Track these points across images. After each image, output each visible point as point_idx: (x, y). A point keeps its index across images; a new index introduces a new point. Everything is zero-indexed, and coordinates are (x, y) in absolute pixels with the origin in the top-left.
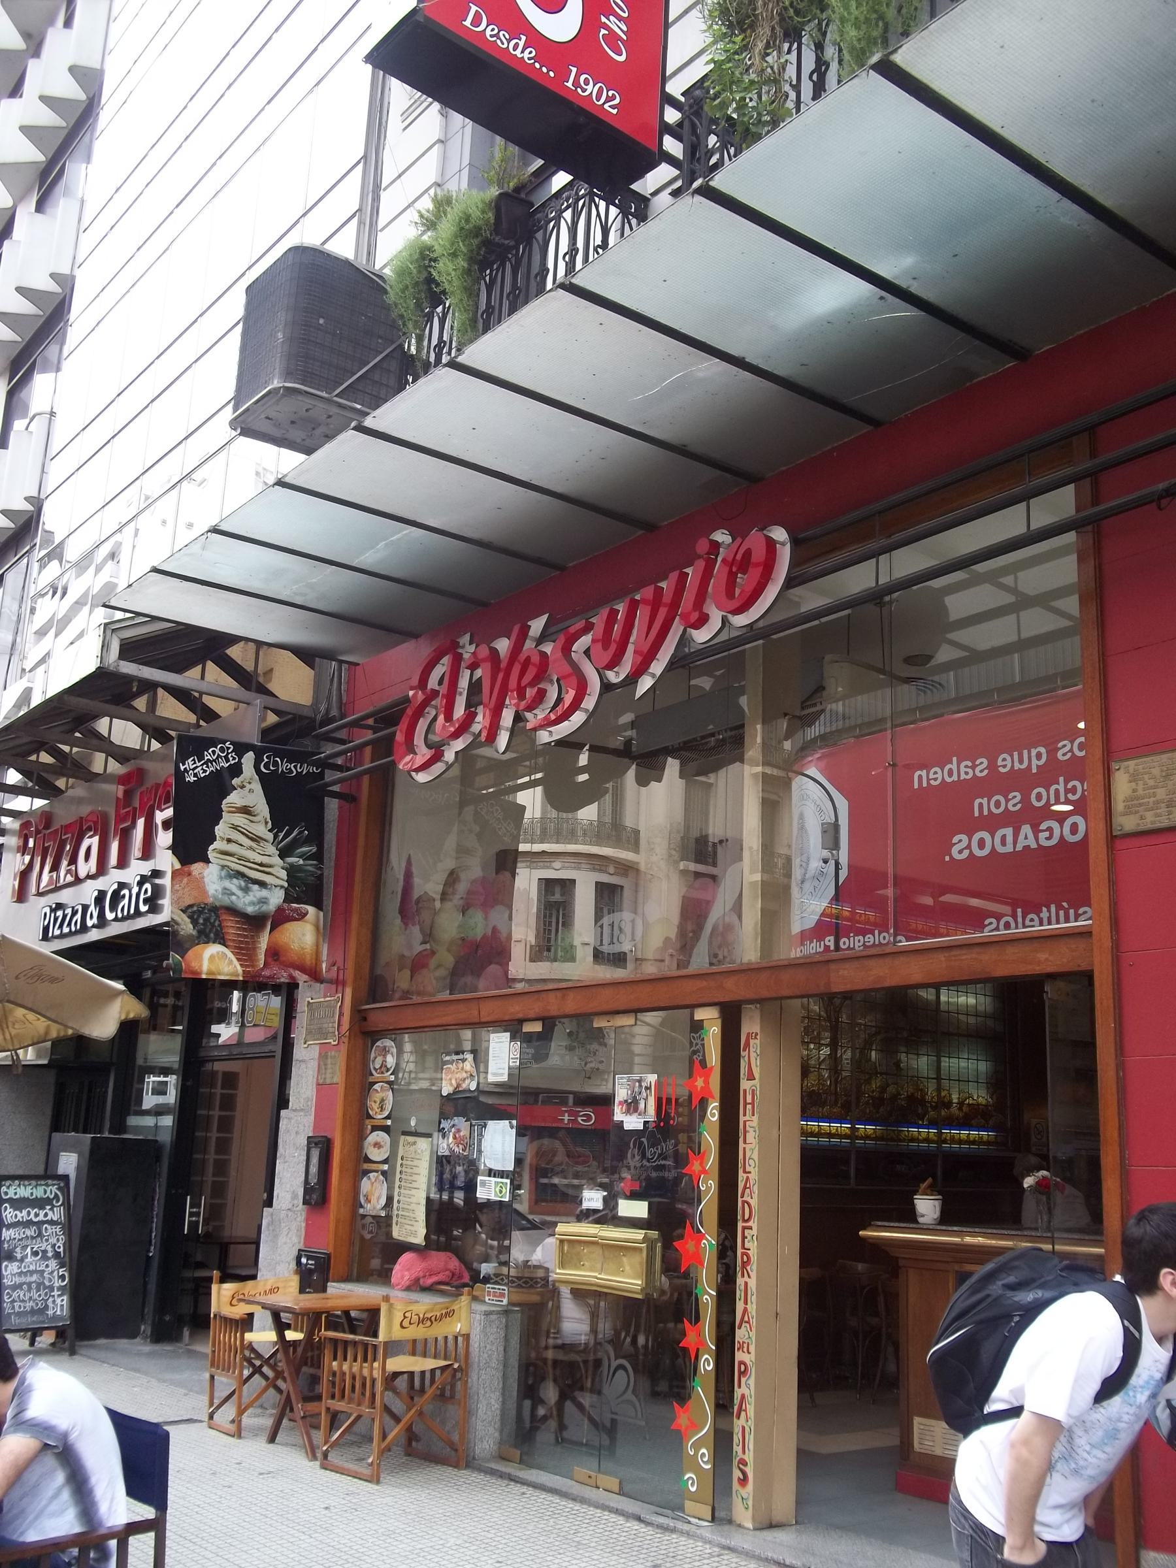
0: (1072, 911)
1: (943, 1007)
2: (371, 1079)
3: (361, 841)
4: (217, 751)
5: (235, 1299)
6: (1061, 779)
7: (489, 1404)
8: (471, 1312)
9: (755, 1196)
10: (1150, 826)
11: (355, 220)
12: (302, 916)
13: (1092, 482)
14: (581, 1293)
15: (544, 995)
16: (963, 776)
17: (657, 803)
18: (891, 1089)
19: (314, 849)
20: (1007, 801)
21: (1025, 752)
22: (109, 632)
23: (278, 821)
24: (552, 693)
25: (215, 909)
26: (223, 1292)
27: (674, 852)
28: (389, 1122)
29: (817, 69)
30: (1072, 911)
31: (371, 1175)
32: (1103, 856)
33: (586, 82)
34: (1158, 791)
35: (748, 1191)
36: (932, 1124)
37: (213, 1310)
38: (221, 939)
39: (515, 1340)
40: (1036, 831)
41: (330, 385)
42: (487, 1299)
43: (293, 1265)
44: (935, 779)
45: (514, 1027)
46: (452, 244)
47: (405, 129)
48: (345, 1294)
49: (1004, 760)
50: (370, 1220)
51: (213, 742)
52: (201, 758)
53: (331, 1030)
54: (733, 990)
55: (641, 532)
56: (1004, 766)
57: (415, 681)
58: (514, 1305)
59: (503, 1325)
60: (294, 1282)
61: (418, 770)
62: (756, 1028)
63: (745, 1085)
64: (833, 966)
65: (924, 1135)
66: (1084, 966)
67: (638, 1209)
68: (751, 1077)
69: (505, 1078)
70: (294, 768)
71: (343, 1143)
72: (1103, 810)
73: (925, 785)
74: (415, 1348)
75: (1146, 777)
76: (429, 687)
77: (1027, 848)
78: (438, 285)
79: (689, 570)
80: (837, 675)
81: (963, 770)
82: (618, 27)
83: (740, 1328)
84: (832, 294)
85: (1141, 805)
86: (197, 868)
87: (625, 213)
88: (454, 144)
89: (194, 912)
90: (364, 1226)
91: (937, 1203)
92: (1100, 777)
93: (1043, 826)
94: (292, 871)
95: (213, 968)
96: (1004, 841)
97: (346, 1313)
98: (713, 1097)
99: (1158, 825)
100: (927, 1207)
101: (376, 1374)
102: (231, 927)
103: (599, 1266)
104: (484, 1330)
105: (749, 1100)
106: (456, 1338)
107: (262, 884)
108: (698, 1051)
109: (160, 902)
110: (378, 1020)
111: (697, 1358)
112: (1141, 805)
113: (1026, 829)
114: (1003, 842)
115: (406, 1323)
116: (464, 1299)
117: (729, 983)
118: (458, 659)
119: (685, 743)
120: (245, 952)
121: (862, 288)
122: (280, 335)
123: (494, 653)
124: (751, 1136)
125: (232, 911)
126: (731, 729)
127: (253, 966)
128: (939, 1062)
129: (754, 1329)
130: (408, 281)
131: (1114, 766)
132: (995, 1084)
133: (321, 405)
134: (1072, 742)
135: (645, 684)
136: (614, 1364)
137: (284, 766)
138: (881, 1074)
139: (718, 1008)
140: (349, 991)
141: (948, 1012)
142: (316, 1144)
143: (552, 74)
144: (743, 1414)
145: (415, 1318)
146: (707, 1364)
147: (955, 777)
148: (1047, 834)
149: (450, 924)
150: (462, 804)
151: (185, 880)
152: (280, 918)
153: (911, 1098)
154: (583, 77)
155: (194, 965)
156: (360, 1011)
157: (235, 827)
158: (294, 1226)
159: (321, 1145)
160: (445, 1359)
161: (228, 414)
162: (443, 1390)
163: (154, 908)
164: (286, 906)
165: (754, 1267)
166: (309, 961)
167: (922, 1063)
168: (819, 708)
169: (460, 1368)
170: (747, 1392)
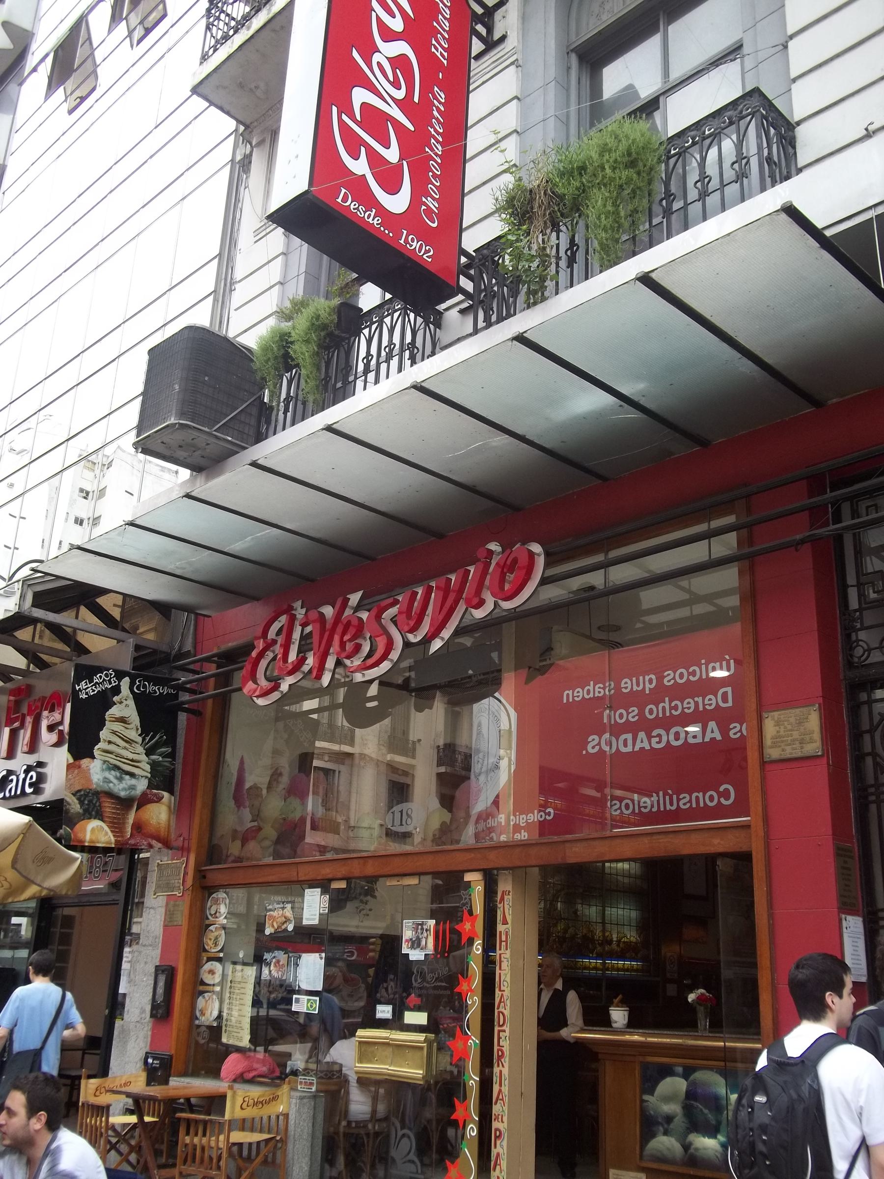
0: (675, 797)
1: (607, 871)
2: (207, 922)
3: (205, 744)
4: (103, 676)
5: (97, 1092)
6: (667, 699)
7: (301, 1167)
8: (290, 1097)
9: (508, 1008)
10: (789, 756)
11: (212, 297)
12: (159, 799)
13: (747, 531)
14: (364, 1081)
15: (349, 862)
16: (597, 694)
17: (428, 724)
18: (571, 931)
19: (169, 750)
20: (628, 713)
21: (641, 678)
22: (25, 587)
23: (146, 729)
24: (366, 648)
25: (97, 793)
26: (90, 1086)
27: (382, 747)
28: (221, 955)
29: (571, 248)
30: (675, 797)
31: (206, 995)
32: (757, 774)
33: (413, 240)
34: (794, 733)
35: (502, 1004)
36: (599, 956)
37: (81, 1100)
38: (100, 816)
39: (320, 1117)
40: (649, 737)
41: (212, 423)
42: (299, 1087)
43: (140, 1065)
44: (578, 696)
45: (324, 885)
46: (307, 334)
47: (256, 242)
48: (182, 1085)
49: (626, 683)
50: (204, 1029)
51: (100, 670)
52: (91, 681)
53: (177, 885)
54: (493, 860)
55: (433, 539)
56: (626, 688)
57: (259, 630)
58: (322, 1092)
59: (312, 1107)
60: (143, 1077)
61: (258, 697)
62: (509, 887)
63: (500, 928)
64: (567, 845)
65: (593, 965)
66: (745, 848)
67: (419, 1018)
68: (505, 922)
69: (316, 922)
70: (158, 690)
71: (185, 970)
72: (757, 743)
73: (571, 700)
74: (244, 1125)
75: (786, 723)
76: (269, 637)
77: (642, 749)
78: (293, 360)
79: (472, 569)
80: (562, 642)
81: (597, 690)
82: (433, 205)
83: (496, 1103)
84: (589, 401)
85: (783, 742)
86: (85, 762)
87: (427, 323)
88: (294, 257)
89: (81, 796)
90: (199, 1034)
91: (626, 1013)
92: (755, 722)
93: (654, 733)
94: (154, 765)
95: (94, 838)
96: (626, 744)
97: (188, 1100)
98: (478, 937)
99: (794, 755)
100: (619, 1016)
101: (221, 1145)
102: (108, 807)
103: (390, 1061)
104: (298, 1111)
105: (504, 938)
106: (278, 1117)
107: (132, 775)
108: (467, 903)
109: (42, 786)
110: (214, 878)
111: (464, 1127)
112: (783, 742)
113: (642, 735)
114: (625, 745)
115: (244, 1106)
116: (285, 1088)
117: (492, 855)
118: (292, 619)
119: (449, 682)
120: (117, 826)
121: (609, 399)
122: (177, 387)
123: (322, 615)
124: (505, 965)
125: (110, 794)
126: (484, 674)
127: (122, 837)
128: (604, 911)
129: (506, 1105)
130: (270, 355)
131: (765, 715)
132: (642, 927)
133: (204, 437)
134: (675, 673)
135: (436, 645)
136: (400, 1133)
137: (150, 688)
138: (564, 919)
139: (482, 873)
140: (192, 858)
141: (610, 874)
142: (163, 971)
143: (391, 235)
144: (498, 1167)
145: (251, 1102)
146: (472, 1131)
147: (591, 695)
148: (657, 739)
149: (274, 806)
150: (277, 719)
151: (76, 771)
152: (144, 800)
153: (585, 937)
154: (411, 237)
155: (80, 836)
156: (200, 871)
157: (114, 733)
158: (141, 1034)
159: (166, 973)
160: (269, 1132)
161: (132, 437)
162: (266, 1157)
163: (37, 791)
164: (148, 791)
165: (507, 1059)
166: (163, 833)
167: (592, 912)
168: (548, 662)
169: (281, 1140)
170: (501, 1151)
